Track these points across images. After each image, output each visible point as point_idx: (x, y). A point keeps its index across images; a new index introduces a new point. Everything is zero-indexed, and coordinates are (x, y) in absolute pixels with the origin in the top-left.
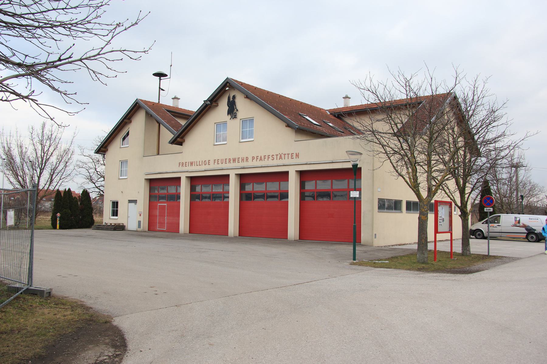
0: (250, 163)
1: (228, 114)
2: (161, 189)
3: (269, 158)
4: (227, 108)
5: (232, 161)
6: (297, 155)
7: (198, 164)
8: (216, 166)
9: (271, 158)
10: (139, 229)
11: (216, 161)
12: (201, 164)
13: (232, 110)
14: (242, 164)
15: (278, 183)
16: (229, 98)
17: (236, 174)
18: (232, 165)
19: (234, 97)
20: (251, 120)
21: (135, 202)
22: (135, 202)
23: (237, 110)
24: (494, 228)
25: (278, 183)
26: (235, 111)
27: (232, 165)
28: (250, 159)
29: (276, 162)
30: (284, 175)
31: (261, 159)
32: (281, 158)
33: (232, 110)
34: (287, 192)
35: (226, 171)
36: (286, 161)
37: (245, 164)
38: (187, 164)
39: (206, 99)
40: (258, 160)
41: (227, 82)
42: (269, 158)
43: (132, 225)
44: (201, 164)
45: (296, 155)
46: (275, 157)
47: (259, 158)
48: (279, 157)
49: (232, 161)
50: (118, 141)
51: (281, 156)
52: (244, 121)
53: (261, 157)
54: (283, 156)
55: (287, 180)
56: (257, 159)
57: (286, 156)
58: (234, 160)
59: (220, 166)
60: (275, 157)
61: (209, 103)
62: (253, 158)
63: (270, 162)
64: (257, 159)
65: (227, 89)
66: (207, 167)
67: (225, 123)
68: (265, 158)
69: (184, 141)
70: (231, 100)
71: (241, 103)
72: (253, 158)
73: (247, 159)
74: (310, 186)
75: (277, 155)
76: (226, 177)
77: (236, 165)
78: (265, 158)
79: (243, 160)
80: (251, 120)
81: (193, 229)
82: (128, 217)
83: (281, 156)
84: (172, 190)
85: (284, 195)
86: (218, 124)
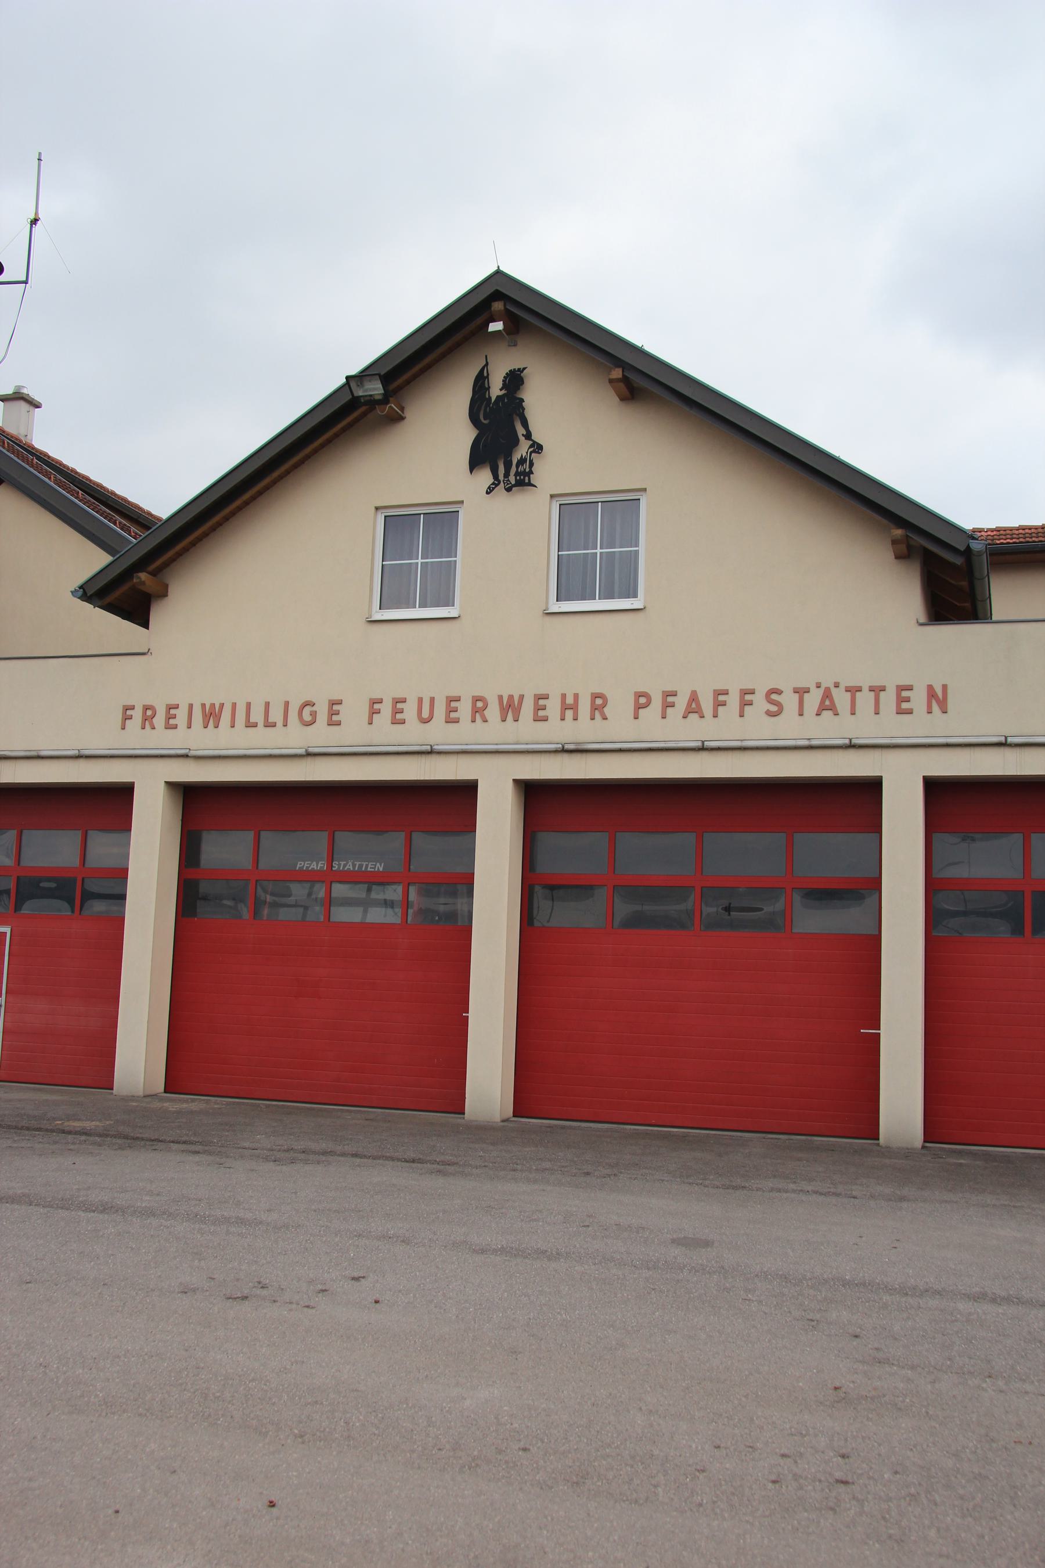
1: (475, 463)
3: (744, 704)
4: (465, 435)
5: (493, 712)
6: (938, 699)
7: (257, 716)
8: (651, 727)
11: (386, 709)
12: (276, 715)
13: (500, 442)
14: (559, 730)
15: (250, 835)
16: (481, 383)
17: (170, 784)
18: (494, 731)
19: (515, 380)
20: (624, 507)
23: (538, 448)
25: (78, 835)
26: (523, 449)
27: (494, 731)
28: (620, 705)
29: (790, 728)
30: (112, 803)
31: (694, 707)
32: (827, 704)
33: (500, 442)
34: (121, 874)
36: (864, 726)
37: (584, 730)
38: (181, 715)
39: (354, 372)
41: (497, 295)
42: (744, 704)
44: (276, 715)
45: (931, 693)
46: (789, 701)
48: (813, 700)
49: (493, 712)
51: (827, 694)
52: (574, 512)
53: (694, 698)
54: (842, 699)
55: (125, 826)
56: (667, 705)
57: (865, 699)
58: (510, 708)
60: (789, 701)
61: (375, 388)
62: (641, 701)
63: (757, 727)
64: (667, 705)
65: (496, 326)
68: (718, 704)
69: (163, 594)
70: (496, 390)
71: (560, 409)
72: (641, 701)
73: (599, 704)
74: (227, 849)
75: (801, 692)
76: (120, 796)
77: (525, 730)
78: (718, 704)
80: (624, 507)
81: (186, 1065)
83: (827, 694)
84: (823, 852)
85: (112, 884)
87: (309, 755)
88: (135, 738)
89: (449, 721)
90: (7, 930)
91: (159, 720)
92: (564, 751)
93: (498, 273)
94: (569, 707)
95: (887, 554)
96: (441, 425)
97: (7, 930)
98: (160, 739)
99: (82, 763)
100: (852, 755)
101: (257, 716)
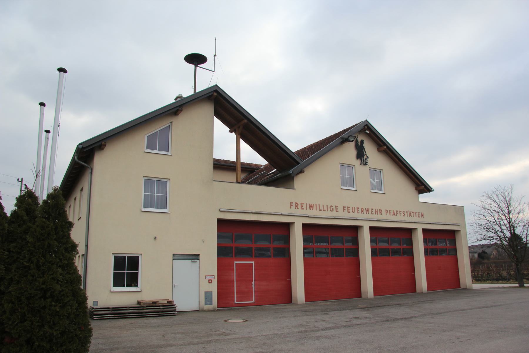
0: (384, 217)
2: (237, 237)
5: (365, 211)
7: (321, 208)
8: (346, 215)
9: (402, 214)
10: (206, 307)
11: (346, 208)
12: (325, 208)
18: (365, 216)
19: (362, 142)
21: (195, 257)
22: (195, 257)
23: (368, 157)
24: (82, 276)
26: (365, 157)
27: (365, 216)
31: (394, 214)
35: (335, 220)
36: (361, 216)
37: (379, 217)
40: (392, 214)
43: (187, 299)
47: (392, 212)
50: (141, 139)
51: (410, 214)
52: (372, 170)
54: (412, 214)
58: (367, 211)
59: (351, 215)
66: (334, 214)
67: (352, 166)
68: (397, 213)
70: (359, 143)
78: (397, 213)
79: (376, 212)
80: (379, 171)
82: (173, 286)
83: (410, 214)
86: (342, 165)
87: (282, 215)
88: (293, 211)
89: (301, 209)
90: (253, 262)
91: (299, 207)
92: (252, 213)
93: (216, 85)
94: (311, 207)
95: (414, 189)
96: (350, 149)
97: (253, 262)
98: (299, 212)
99: (308, 218)
100: (281, 217)
101: (321, 208)
